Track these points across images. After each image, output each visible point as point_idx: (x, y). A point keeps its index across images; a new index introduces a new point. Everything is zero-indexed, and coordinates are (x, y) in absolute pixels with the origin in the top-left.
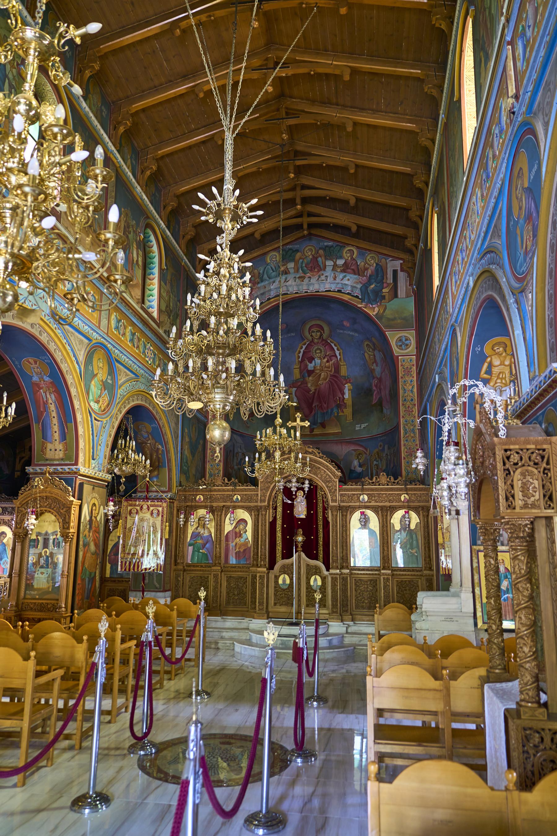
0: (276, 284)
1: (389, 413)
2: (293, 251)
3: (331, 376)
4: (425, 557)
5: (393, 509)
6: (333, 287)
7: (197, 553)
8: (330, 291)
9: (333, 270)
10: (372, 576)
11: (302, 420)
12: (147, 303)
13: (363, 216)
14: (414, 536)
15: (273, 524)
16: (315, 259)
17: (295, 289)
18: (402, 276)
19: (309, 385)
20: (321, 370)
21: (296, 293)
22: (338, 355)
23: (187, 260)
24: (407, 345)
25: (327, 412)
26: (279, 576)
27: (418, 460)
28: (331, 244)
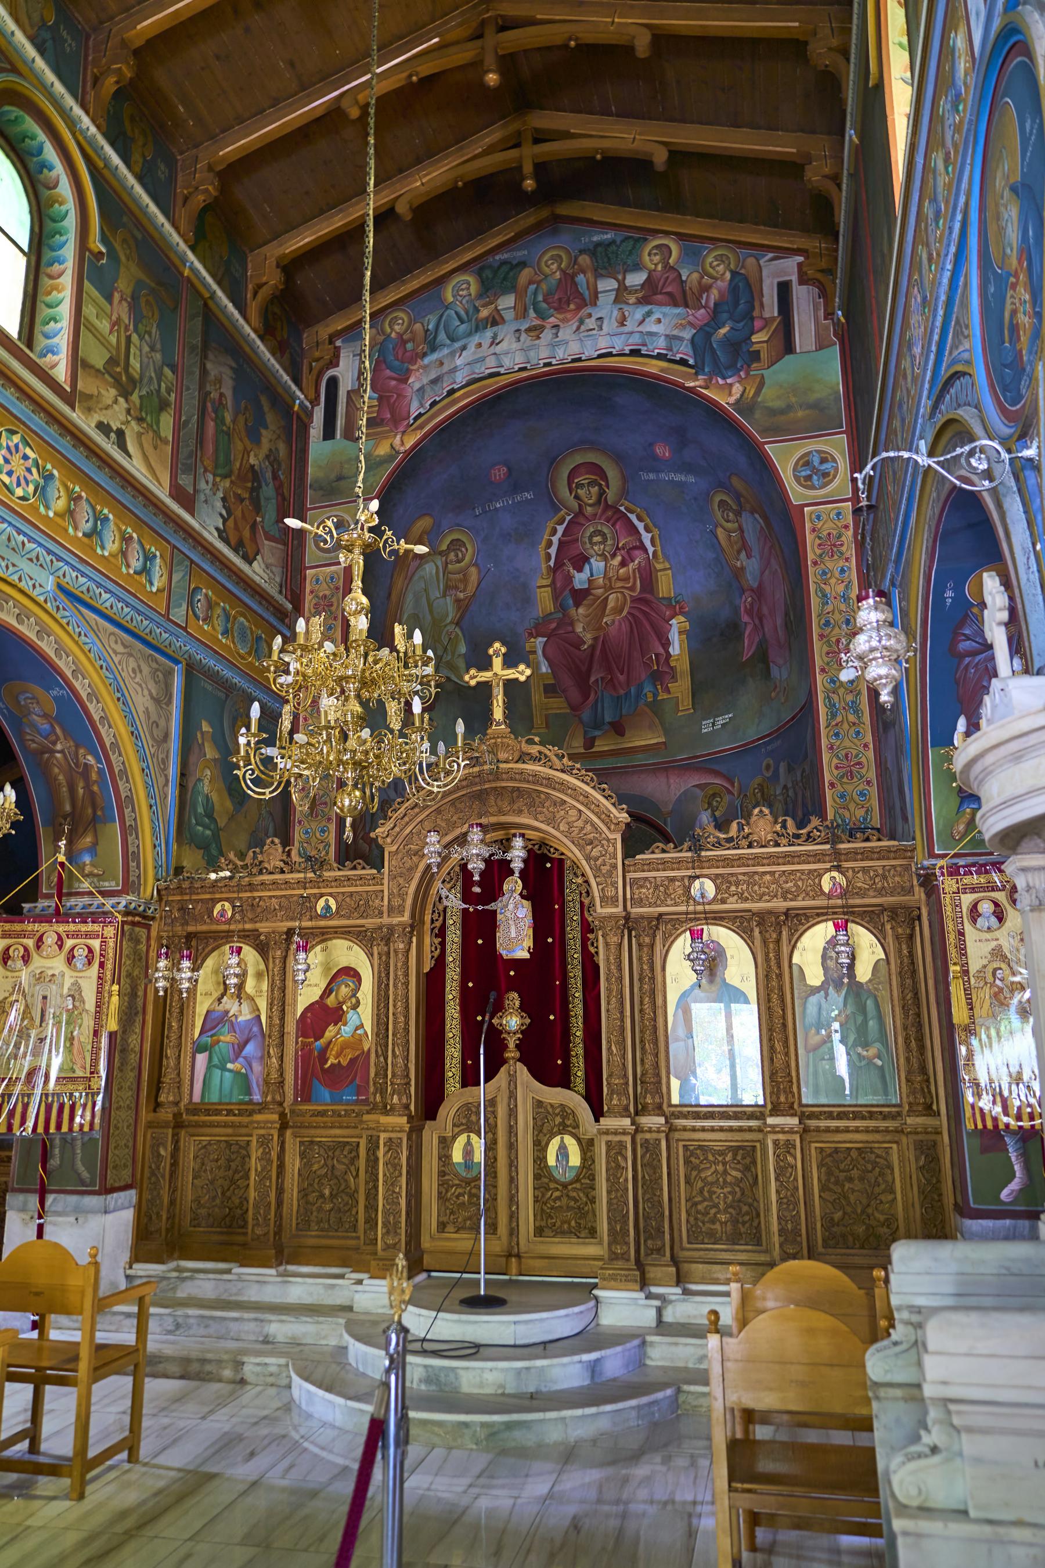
0: (468, 355)
1: (785, 676)
2: (513, 267)
3: (634, 600)
4: (909, 1072)
5: (797, 921)
6: (619, 344)
7: (217, 1073)
8: (610, 355)
9: (616, 301)
10: (738, 1136)
11: (509, 662)
12: (41, 342)
13: (684, 121)
14: (870, 1003)
15: (433, 982)
16: (569, 278)
17: (519, 360)
18: (802, 296)
19: (579, 628)
20: (609, 588)
21: (521, 369)
22: (647, 543)
23: (198, 265)
24: (825, 475)
25: (627, 694)
26: (454, 1138)
27: (862, 643)
28: (609, 236)
